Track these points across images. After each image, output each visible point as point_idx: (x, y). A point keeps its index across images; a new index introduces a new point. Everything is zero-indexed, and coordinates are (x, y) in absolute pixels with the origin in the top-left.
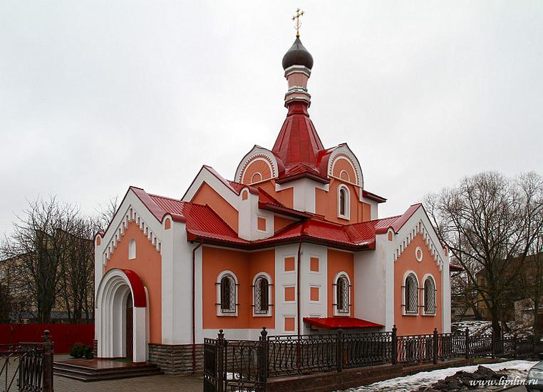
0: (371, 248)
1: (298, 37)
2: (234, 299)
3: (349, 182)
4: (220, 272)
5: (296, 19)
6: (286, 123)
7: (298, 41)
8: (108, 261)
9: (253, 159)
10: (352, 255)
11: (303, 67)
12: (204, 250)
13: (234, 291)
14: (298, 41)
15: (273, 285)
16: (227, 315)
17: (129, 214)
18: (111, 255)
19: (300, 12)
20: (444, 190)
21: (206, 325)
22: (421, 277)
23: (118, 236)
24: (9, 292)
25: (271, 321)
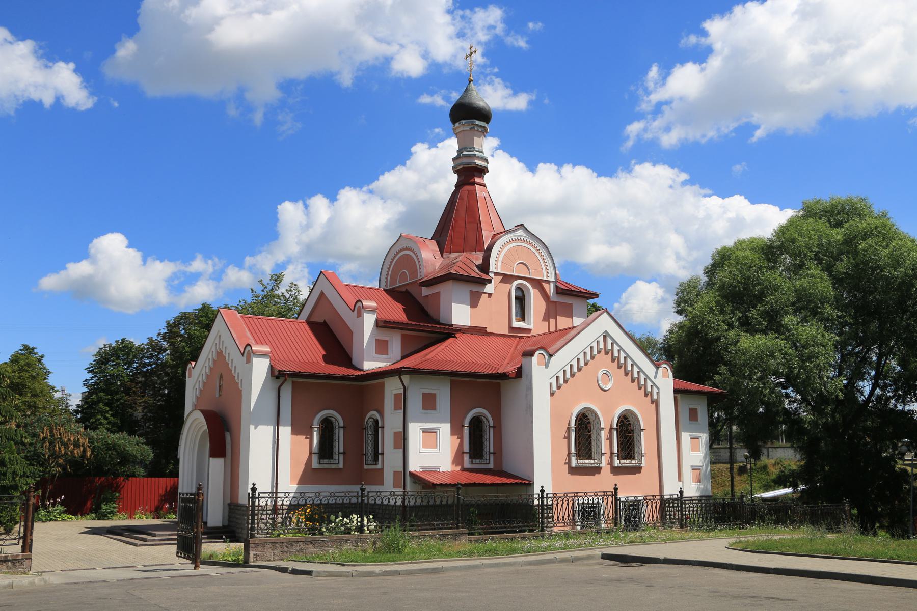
2: (339, 444)
8: (197, 398)
10: (499, 385)
12: (295, 387)
13: (339, 437)
15: (383, 427)
16: (326, 466)
17: (217, 341)
19: (473, 50)
20: (168, 322)
21: (182, 503)
24: (706, 334)
25: (377, 477)
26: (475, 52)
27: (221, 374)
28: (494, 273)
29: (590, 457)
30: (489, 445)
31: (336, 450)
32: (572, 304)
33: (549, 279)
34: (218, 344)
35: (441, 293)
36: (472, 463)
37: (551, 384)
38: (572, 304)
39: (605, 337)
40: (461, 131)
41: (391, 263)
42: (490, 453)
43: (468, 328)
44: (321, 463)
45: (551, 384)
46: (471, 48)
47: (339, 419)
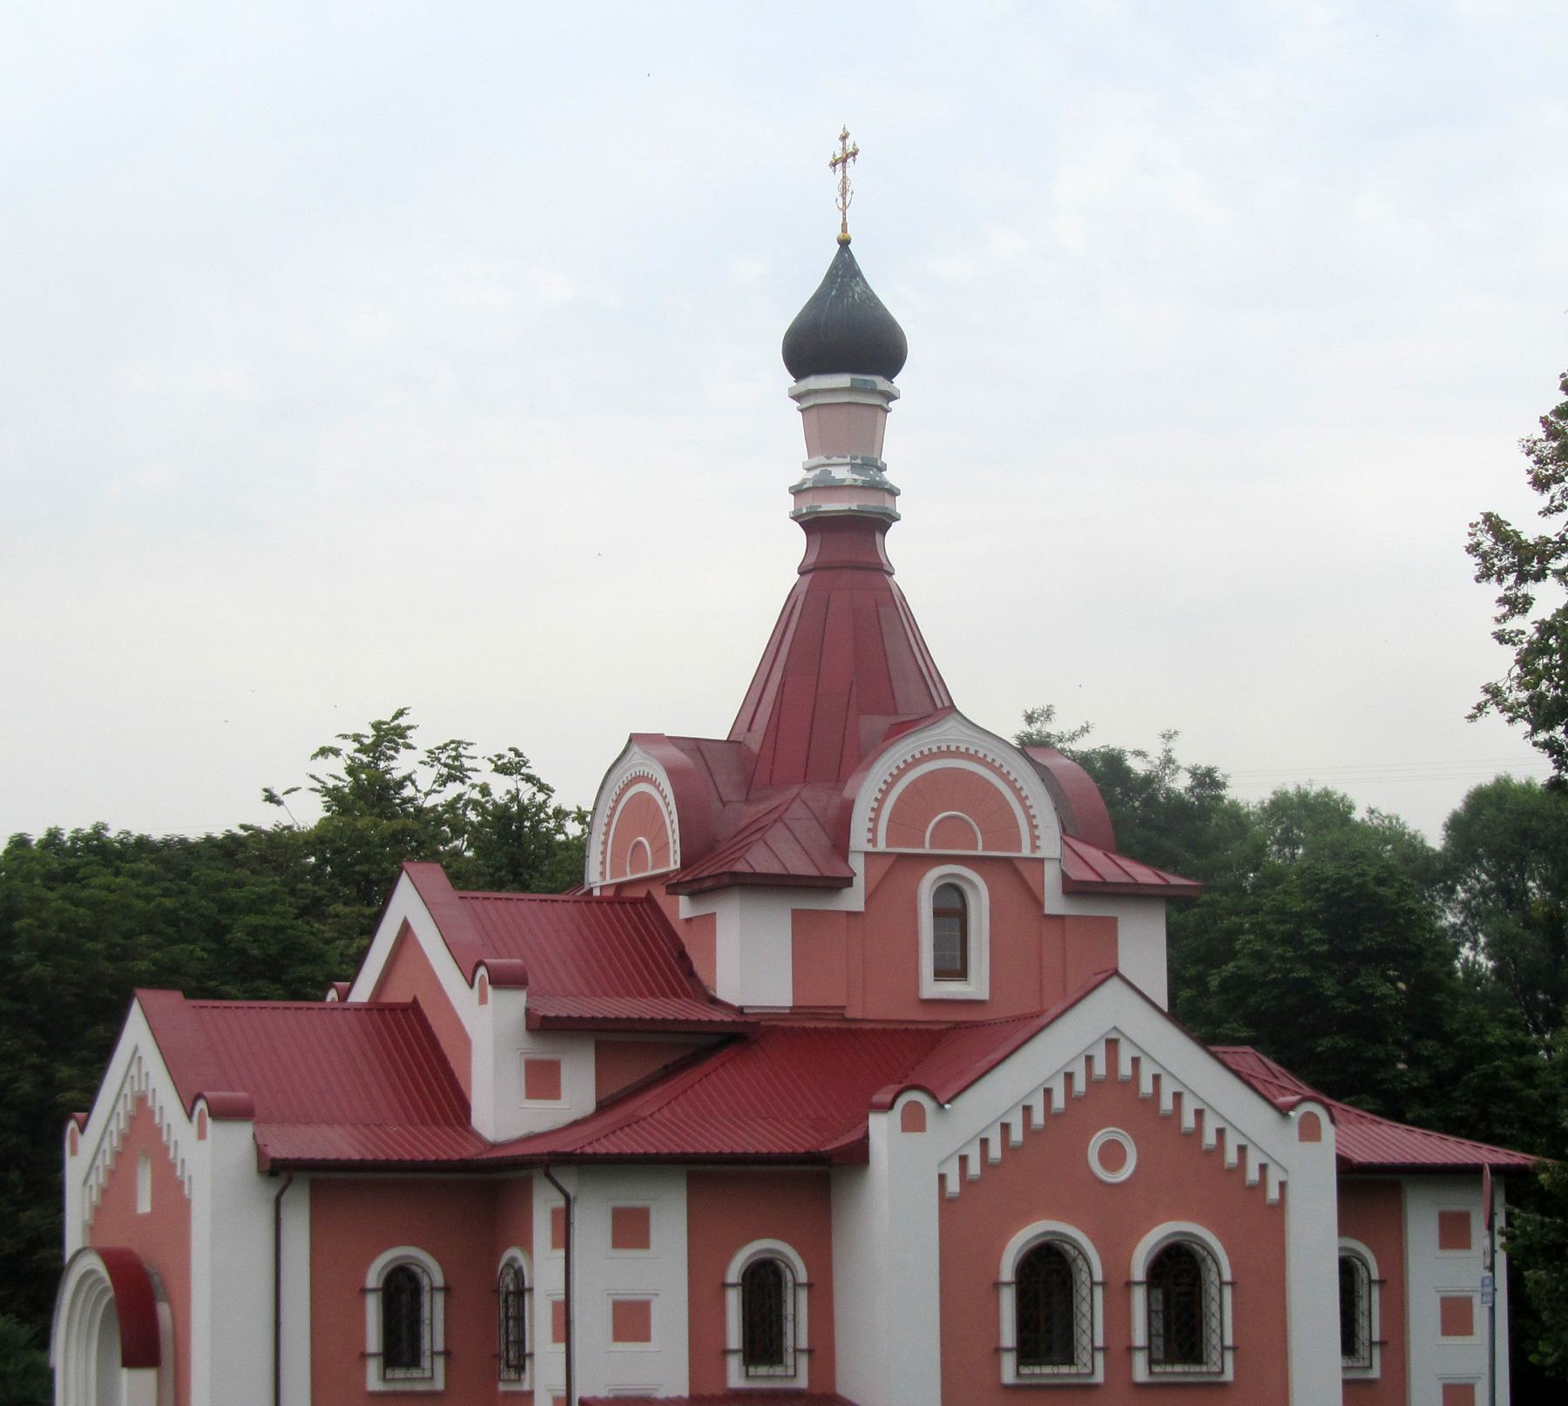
0: (857, 1155)
1: (844, 243)
3: (980, 852)
4: (765, 1236)
5: (839, 166)
6: (792, 601)
7: (844, 269)
9: (620, 796)
11: (843, 380)
13: (434, 1312)
14: (844, 269)
16: (400, 1387)
18: (104, 1192)
22: (1116, 1250)
23: (122, 1115)
26: (854, 154)
27: (414, 748)
28: (867, 854)
29: (1070, 1361)
30: (798, 1330)
31: (426, 1345)
32: (1116, 918)
33: (1038, 855)
34: (136, 1079)
35: (717, 916)
36: (747, 1376)
37: (942, 1178)
38: (1116, 918)
39: (1112, 1045)
40: (812, 406)
41: (614, 809)
42: (1094, 1349)
43: (788, 1011)
44: (750, 1374)
45: (942, 1178)
46: (844, 138)
47: (433, 1272)
